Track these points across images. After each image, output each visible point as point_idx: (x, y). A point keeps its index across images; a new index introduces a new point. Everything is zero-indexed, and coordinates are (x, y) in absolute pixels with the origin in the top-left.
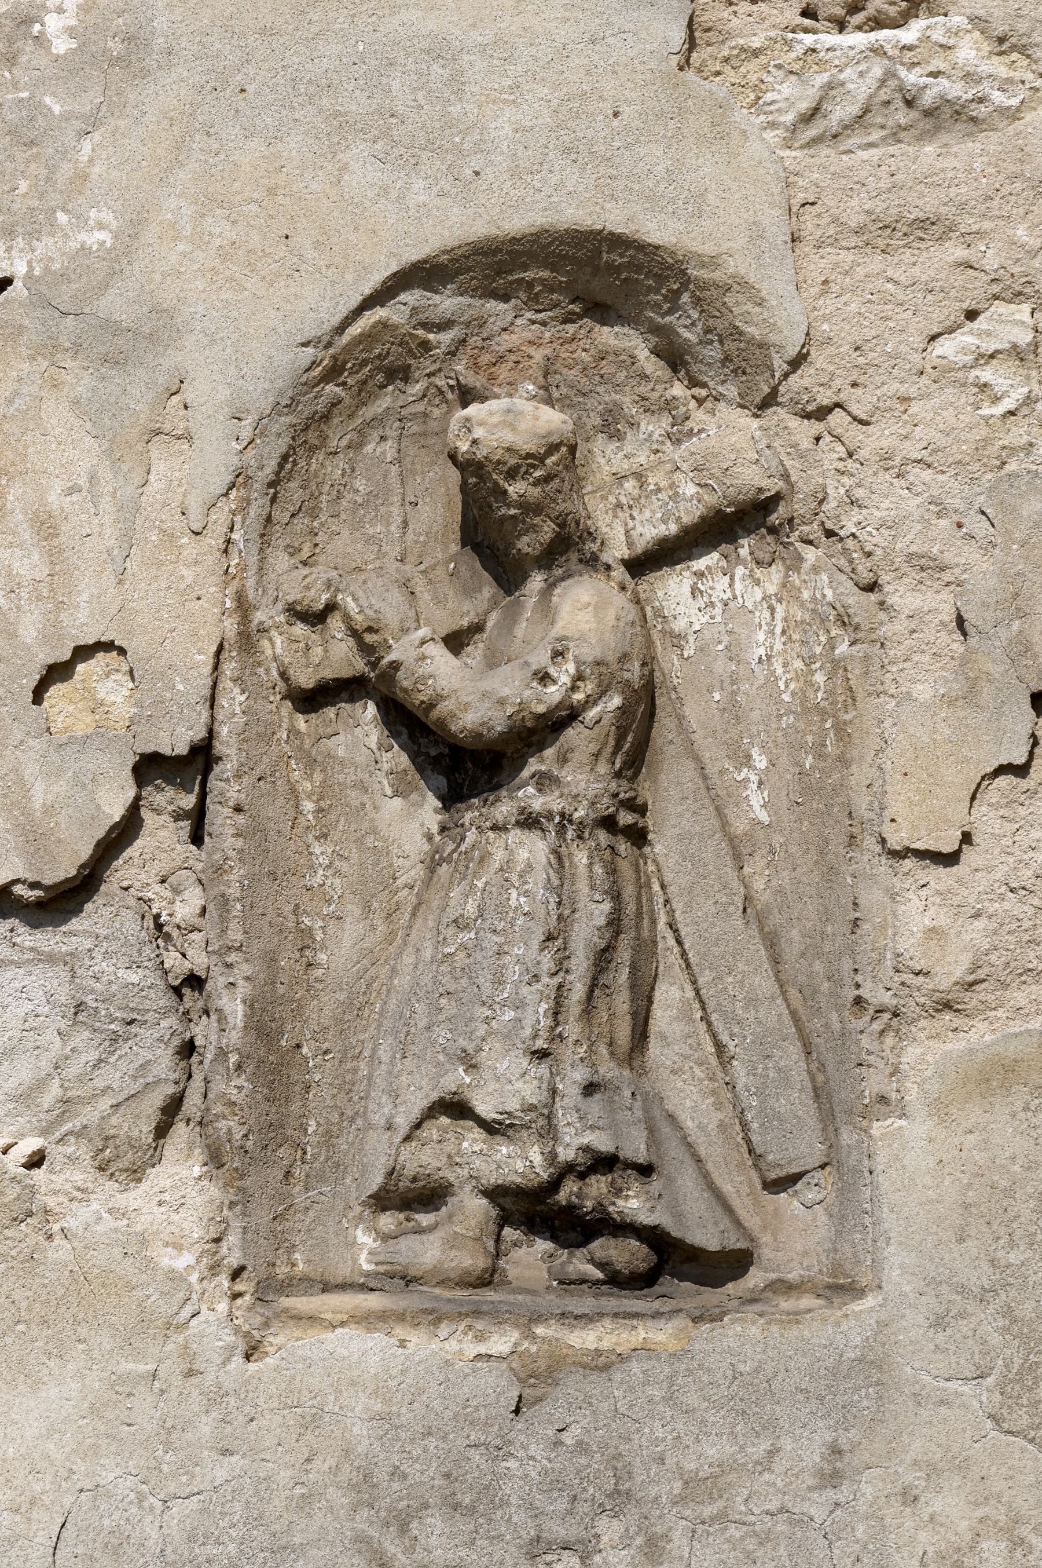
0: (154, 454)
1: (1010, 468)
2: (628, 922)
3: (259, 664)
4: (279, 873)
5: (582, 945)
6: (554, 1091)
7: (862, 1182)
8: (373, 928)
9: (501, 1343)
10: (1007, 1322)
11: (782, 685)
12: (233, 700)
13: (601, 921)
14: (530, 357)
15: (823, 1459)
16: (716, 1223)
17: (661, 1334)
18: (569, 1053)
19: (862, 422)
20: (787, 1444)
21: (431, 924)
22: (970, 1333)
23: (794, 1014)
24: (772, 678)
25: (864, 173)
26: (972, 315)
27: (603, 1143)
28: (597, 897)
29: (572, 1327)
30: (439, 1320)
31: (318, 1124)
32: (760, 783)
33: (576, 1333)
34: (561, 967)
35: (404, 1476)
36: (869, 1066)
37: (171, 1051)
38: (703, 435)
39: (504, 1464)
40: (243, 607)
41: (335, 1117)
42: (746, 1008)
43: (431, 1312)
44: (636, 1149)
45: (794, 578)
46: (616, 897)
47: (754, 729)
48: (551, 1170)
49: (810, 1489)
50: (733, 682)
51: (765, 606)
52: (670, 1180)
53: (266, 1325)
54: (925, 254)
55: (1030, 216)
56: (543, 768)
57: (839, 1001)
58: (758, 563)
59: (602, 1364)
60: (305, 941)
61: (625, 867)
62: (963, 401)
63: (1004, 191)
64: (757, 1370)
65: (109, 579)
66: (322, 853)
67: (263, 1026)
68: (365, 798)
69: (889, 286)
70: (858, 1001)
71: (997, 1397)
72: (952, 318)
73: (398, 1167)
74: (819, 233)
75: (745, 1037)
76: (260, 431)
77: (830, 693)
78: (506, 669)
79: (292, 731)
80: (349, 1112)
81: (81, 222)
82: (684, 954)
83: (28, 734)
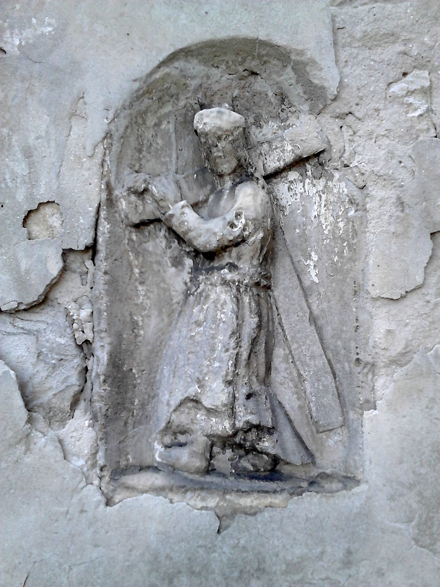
0: (73, 123)
1: (421, 139)
2: (264, 324)
3: (116, 212)
4: (124, 299)
5: (246, 336)
6: (234, 397)
7: (359, 436)
8: (163, 320)
9: (212, 502)
10: (420, 499)
11: (324, 227)
12: (104, 227)
13: (254, 326)
14: (226, 93)
15: (344, 556)
16: (299, 453)
17: (277, 500)
18: (242, 381)
19: (360, 119)
20: (329, 549)
21: (186, 321)
22: (405, 503)
23: (329, 361)
24: (320, 224)
25: (363, 15)
26: (405, 74)
27: (254, 419)
28: (252, 316)
29: (241, 497)
30: (187, 491)
31: (139, 401)
32: (315, 266)
33: (242, 499)
34: (238, 345)
35: (171, 559)
36: (362, 387)
37: (77, 372)
38: (294, 126)
39: (213, 555)
40: (109, 188)
41: (146, 397)
42: (310, 359)
43: (183, 487)
44: (268, 422)
45: (330, 183)
46: (260, 316)
47: (312, 245)
48: (233, 430)
49: (339, 569)
50: (304, 225)
51: (317, 195)
52: (281, 433)
53: (114, 491)
54: (387, 49)
55: (430, 33)
56: (231, 261)
57: (349, 359)
58: (314, 178)
59: (253, 513)
60: (135, 325)
61: (263, 302)
62: (402, 110)
63: (419, 22)
64: (316, 517)
65: (53, 175)
66: (142, 290)
67: (116, 362)
68: (160, 268)
69: (372, 63)
70: (358, 360)
71: (417, 531)
72: (397, 76)
73: (171, 421)
74: (344, 41)
75: (310, 372)
76: (116, 116)
77: (346, 231)
78: (216, 220)
79: (130, 240)
80: (152, 394)
81: (42, 23)
82: (285, 335)
83: (19, 240)
